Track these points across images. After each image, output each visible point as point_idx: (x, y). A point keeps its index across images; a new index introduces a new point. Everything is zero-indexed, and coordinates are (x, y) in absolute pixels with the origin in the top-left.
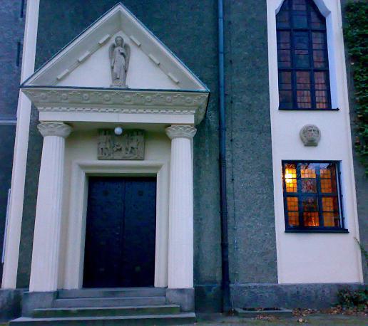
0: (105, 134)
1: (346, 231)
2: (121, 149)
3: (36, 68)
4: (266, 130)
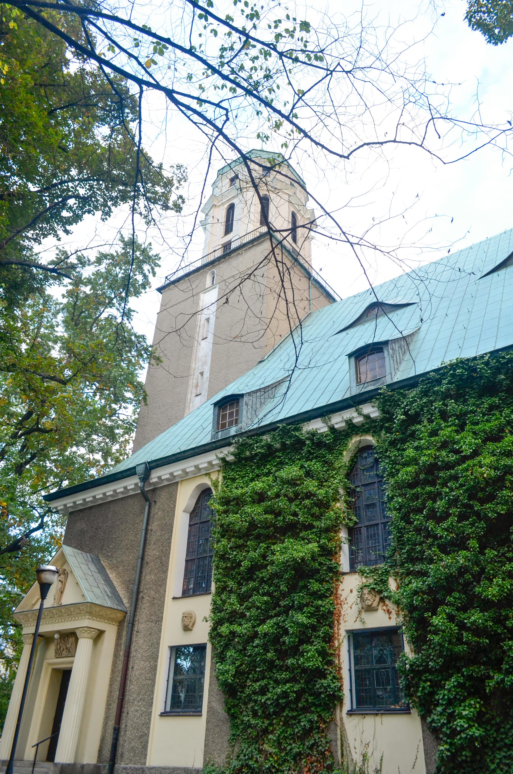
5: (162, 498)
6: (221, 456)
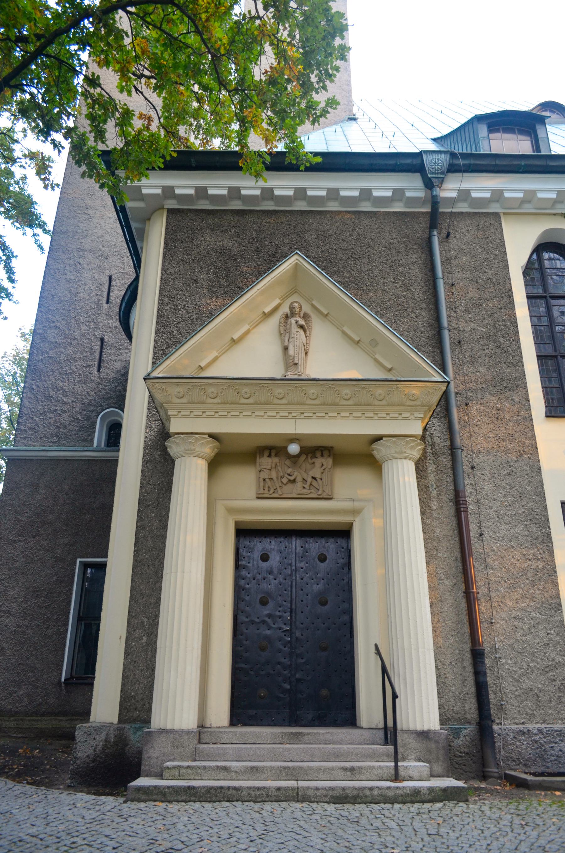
0: (270, 456)
2: (294, 481)
3: (154, 363)
5: (464, 234)
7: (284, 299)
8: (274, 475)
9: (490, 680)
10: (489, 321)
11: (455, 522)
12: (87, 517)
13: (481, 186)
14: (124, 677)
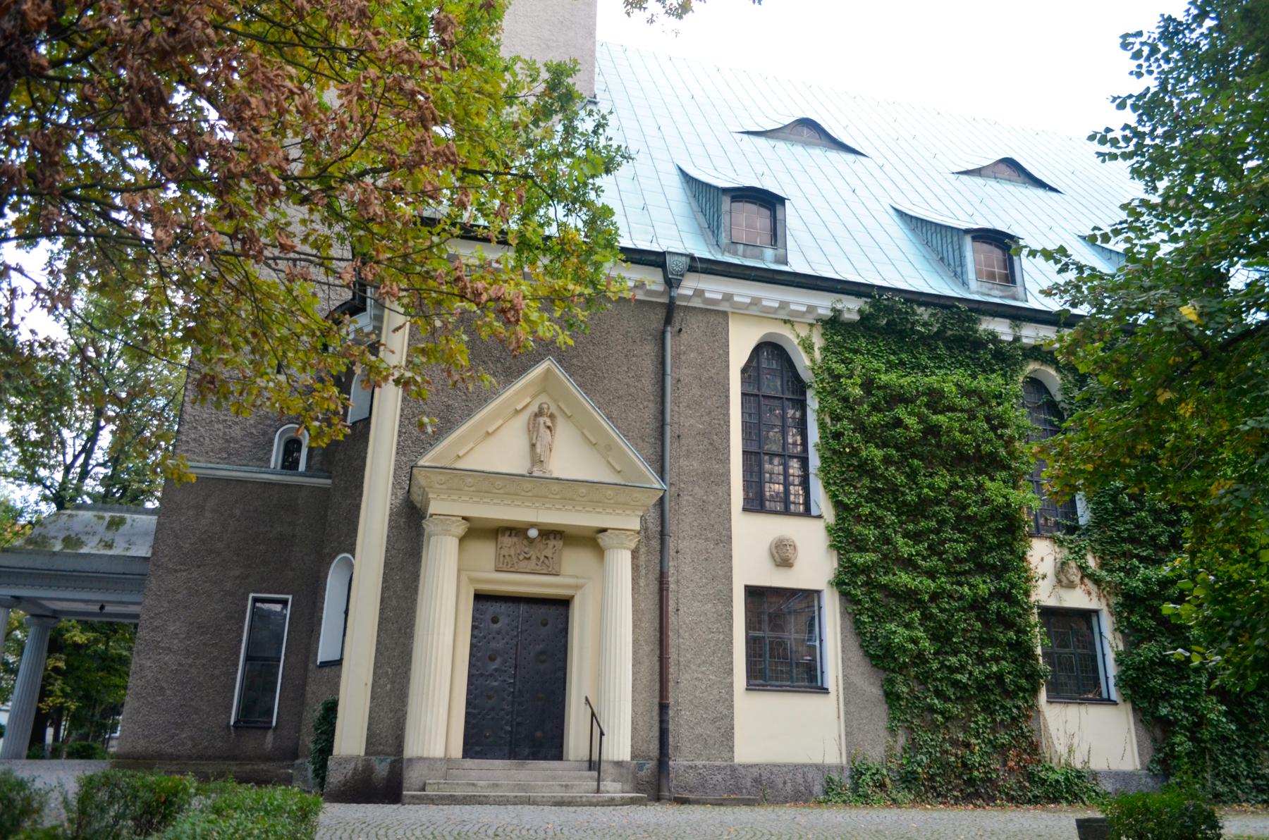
1: (825, 691)
4: (725, 540)
5: (694, 329)
6: (839, 306)
7: (534, 397)
8: (512, 552)
9: (671, 727)
10: (706, 418)
11: (657, 598)
12: (262, 547)
13: (714, 288)
14: (370, 718)
